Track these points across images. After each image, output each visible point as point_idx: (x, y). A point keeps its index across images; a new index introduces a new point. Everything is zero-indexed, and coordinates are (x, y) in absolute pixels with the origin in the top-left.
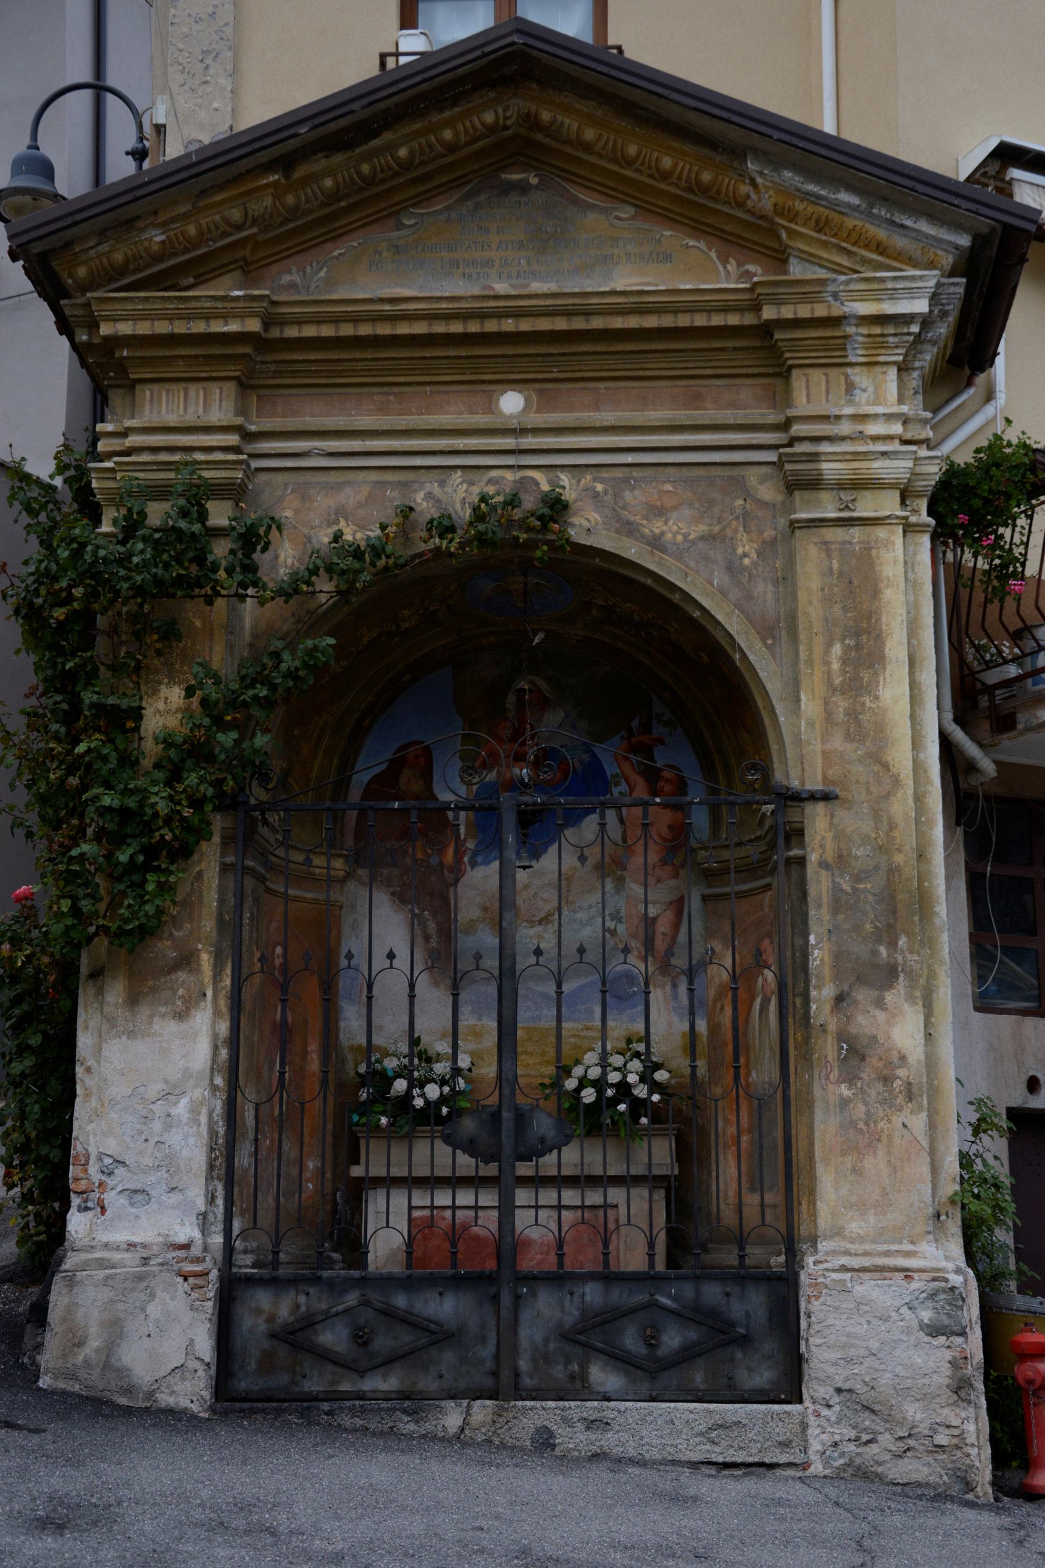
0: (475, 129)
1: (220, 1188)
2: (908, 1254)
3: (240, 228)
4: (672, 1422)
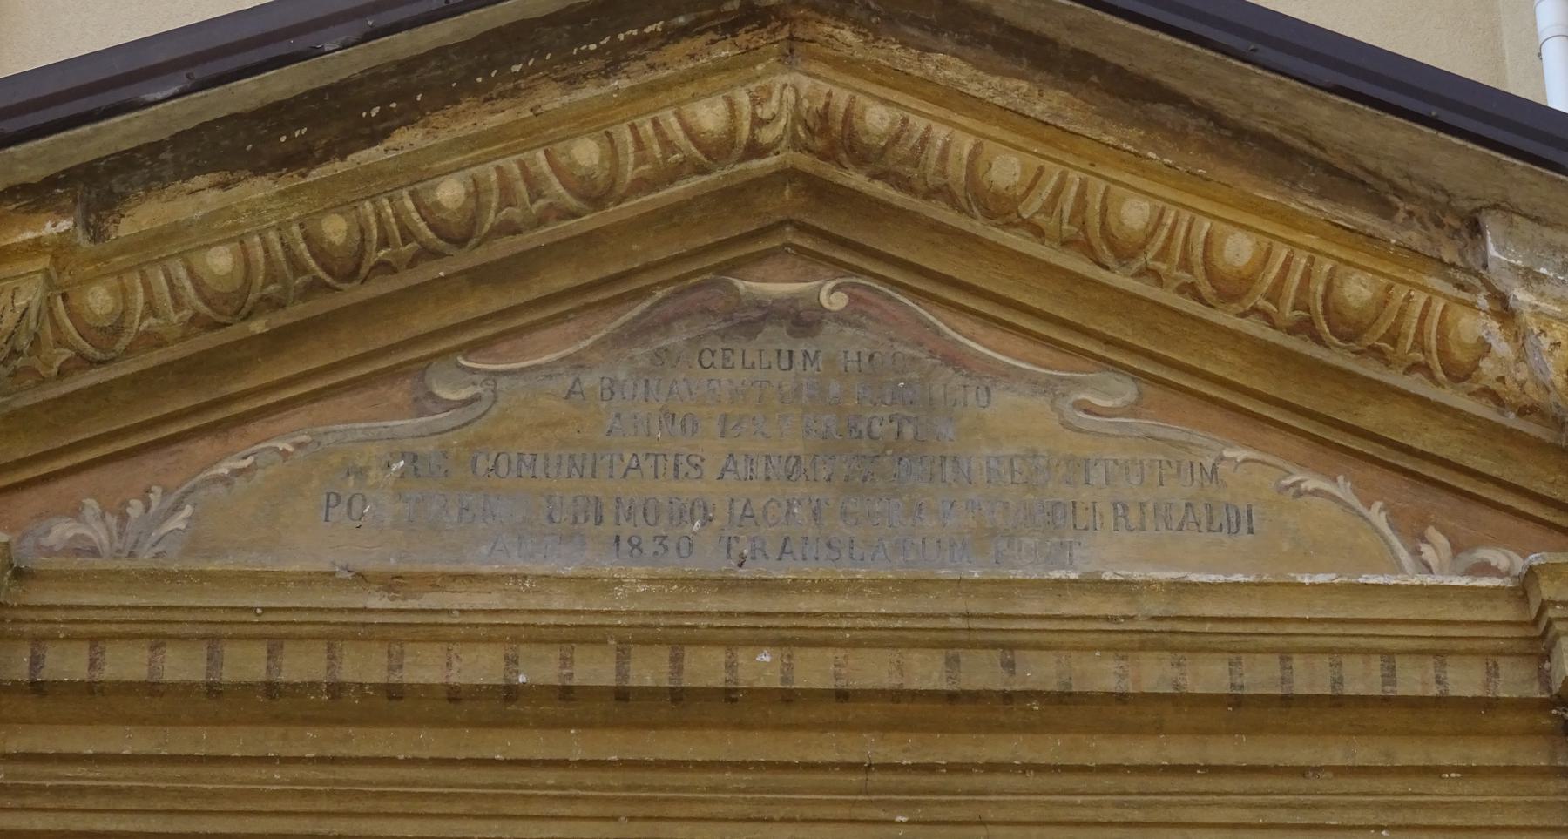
0: (668, 144)
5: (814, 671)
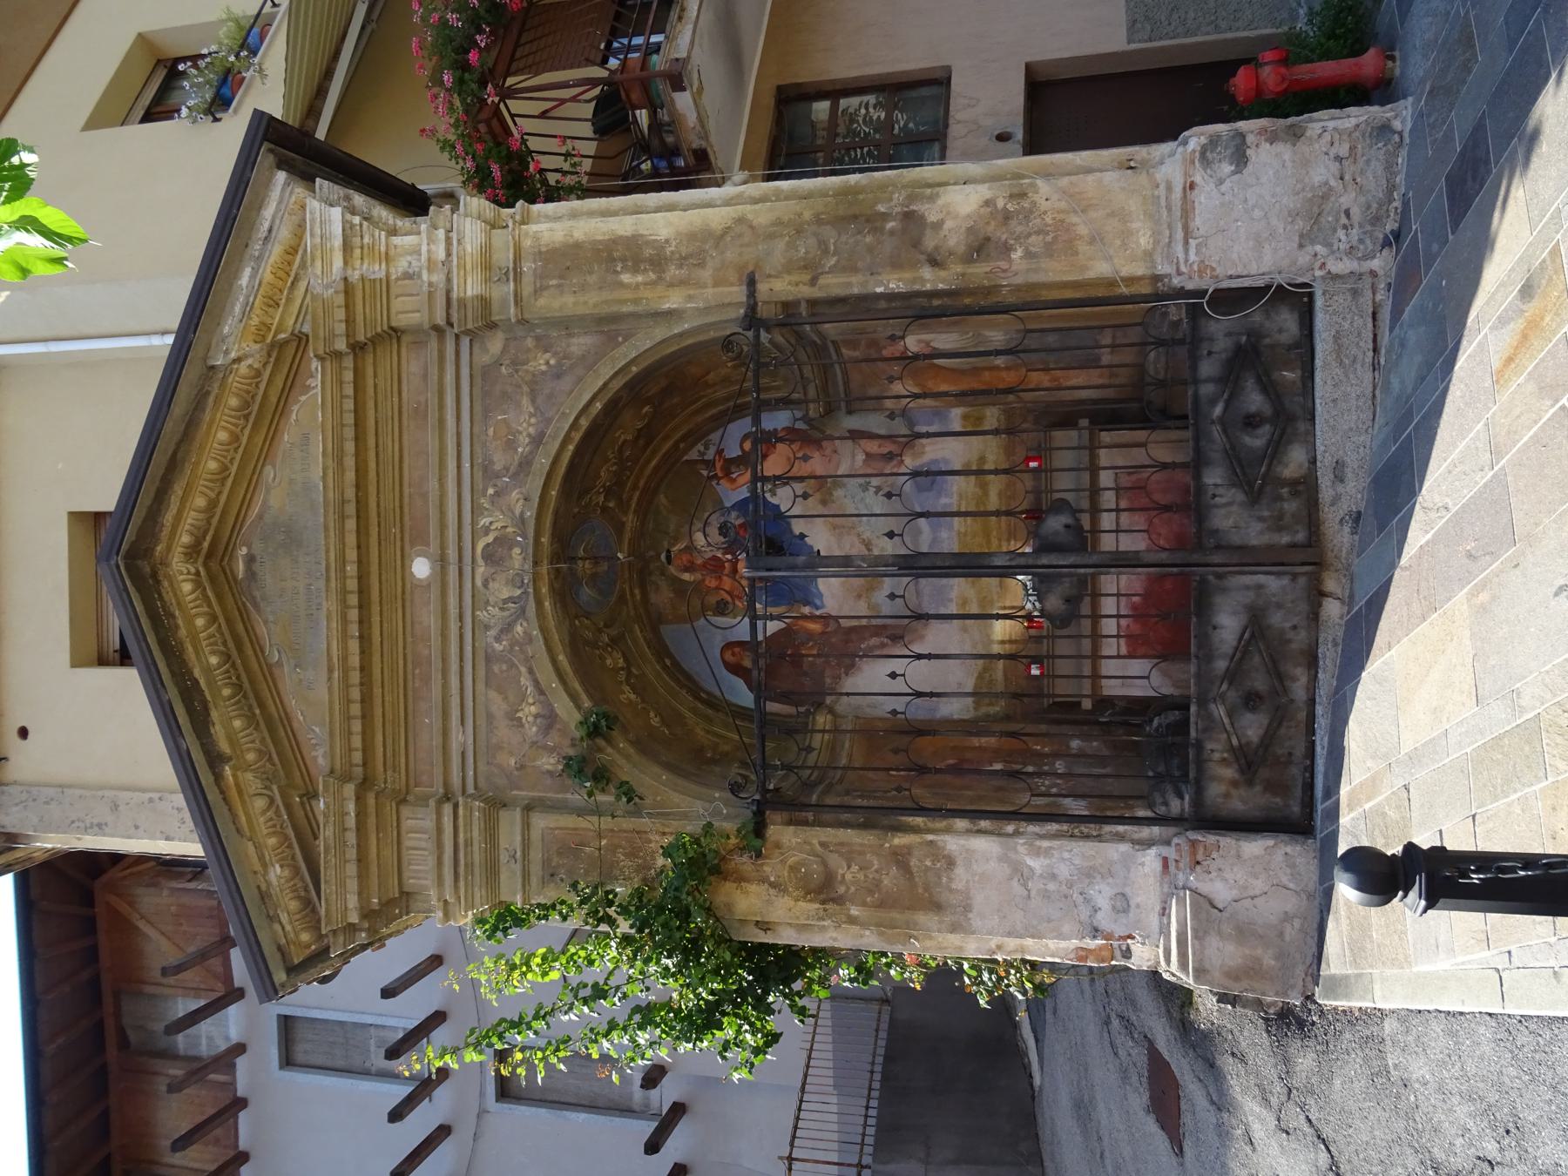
1: (1107, 828)
2: (1169, 188)
3: (272, 801)
4: (1334, 401)
5: (352, 555)
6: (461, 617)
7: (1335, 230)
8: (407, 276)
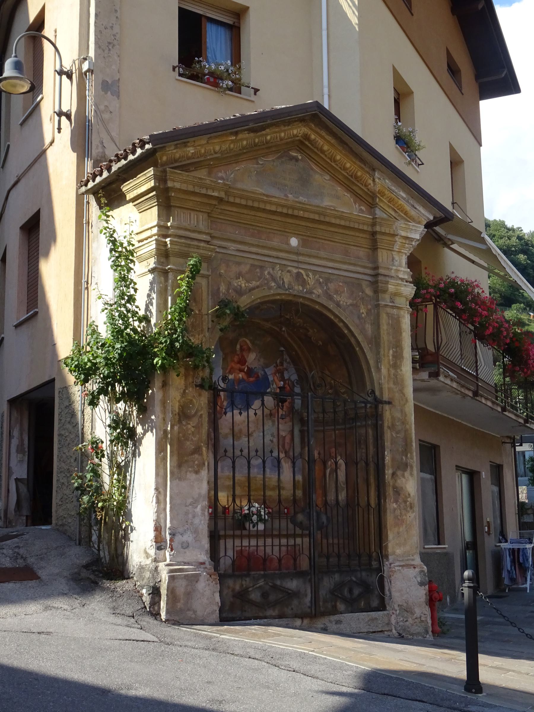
2: (413, 560)
5: (306, 215)
6: (277, 258)
7: (403, 617)
8: (393, 259)
